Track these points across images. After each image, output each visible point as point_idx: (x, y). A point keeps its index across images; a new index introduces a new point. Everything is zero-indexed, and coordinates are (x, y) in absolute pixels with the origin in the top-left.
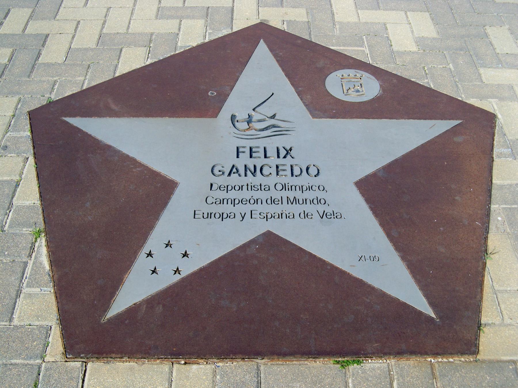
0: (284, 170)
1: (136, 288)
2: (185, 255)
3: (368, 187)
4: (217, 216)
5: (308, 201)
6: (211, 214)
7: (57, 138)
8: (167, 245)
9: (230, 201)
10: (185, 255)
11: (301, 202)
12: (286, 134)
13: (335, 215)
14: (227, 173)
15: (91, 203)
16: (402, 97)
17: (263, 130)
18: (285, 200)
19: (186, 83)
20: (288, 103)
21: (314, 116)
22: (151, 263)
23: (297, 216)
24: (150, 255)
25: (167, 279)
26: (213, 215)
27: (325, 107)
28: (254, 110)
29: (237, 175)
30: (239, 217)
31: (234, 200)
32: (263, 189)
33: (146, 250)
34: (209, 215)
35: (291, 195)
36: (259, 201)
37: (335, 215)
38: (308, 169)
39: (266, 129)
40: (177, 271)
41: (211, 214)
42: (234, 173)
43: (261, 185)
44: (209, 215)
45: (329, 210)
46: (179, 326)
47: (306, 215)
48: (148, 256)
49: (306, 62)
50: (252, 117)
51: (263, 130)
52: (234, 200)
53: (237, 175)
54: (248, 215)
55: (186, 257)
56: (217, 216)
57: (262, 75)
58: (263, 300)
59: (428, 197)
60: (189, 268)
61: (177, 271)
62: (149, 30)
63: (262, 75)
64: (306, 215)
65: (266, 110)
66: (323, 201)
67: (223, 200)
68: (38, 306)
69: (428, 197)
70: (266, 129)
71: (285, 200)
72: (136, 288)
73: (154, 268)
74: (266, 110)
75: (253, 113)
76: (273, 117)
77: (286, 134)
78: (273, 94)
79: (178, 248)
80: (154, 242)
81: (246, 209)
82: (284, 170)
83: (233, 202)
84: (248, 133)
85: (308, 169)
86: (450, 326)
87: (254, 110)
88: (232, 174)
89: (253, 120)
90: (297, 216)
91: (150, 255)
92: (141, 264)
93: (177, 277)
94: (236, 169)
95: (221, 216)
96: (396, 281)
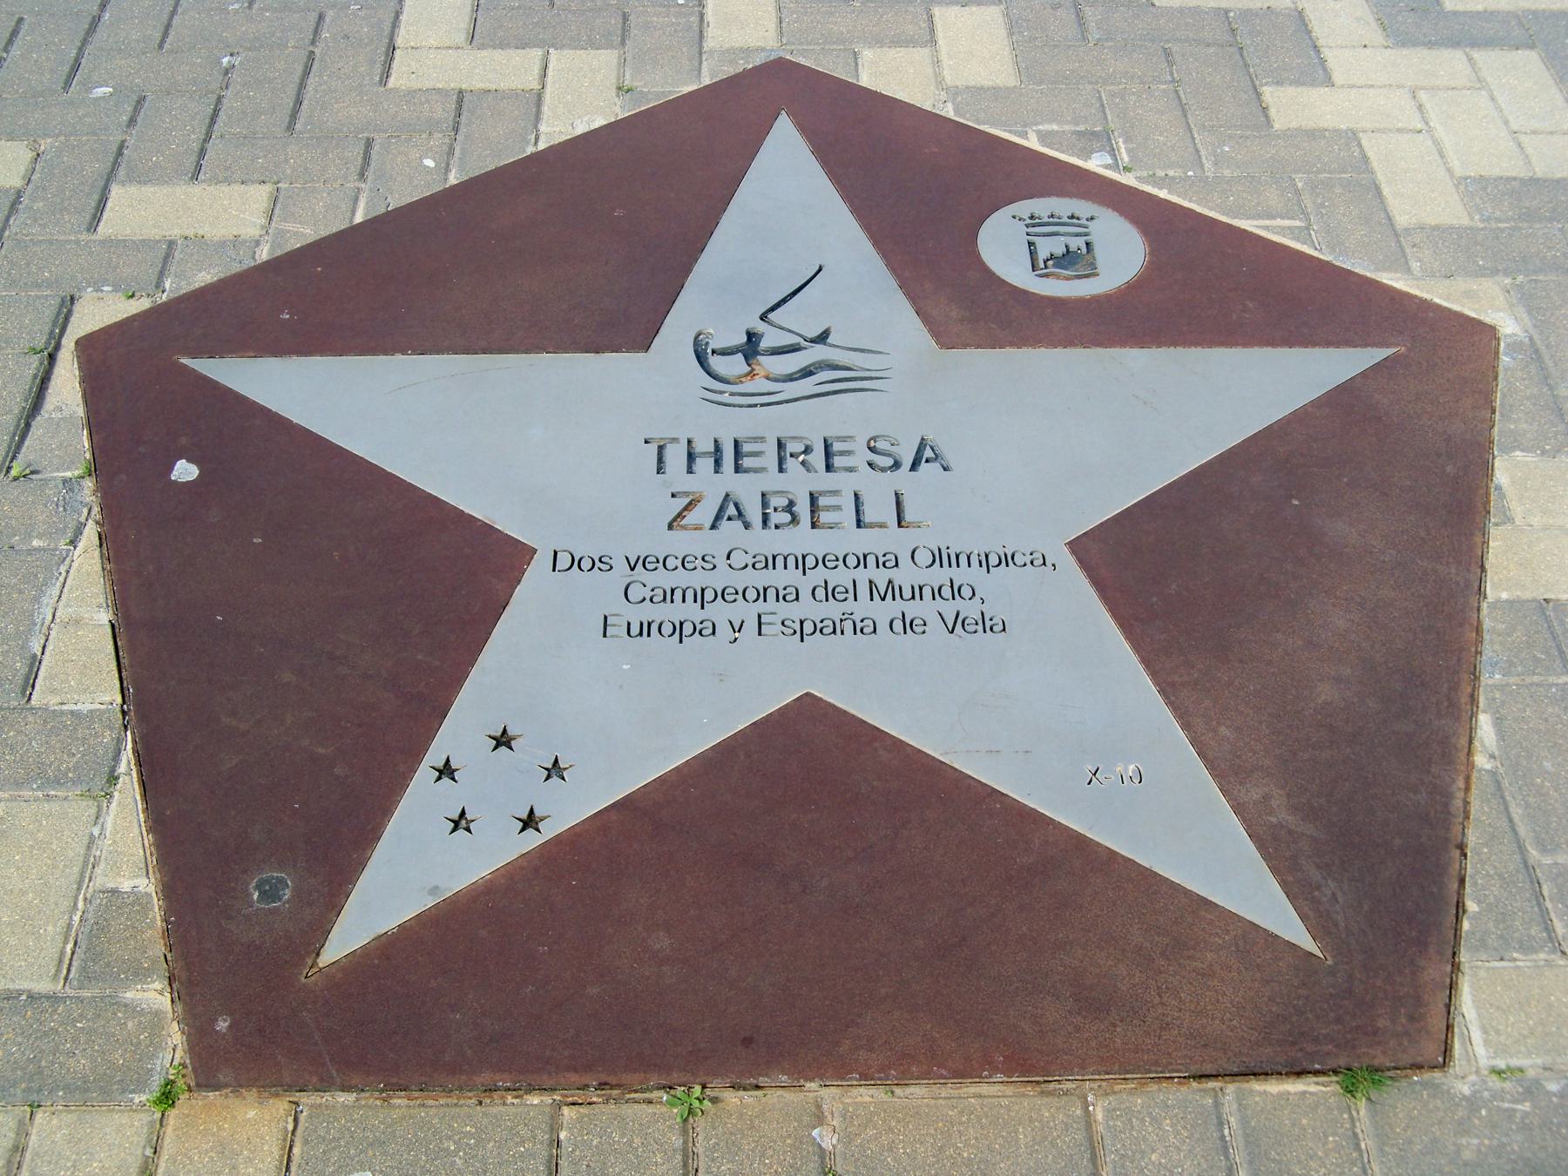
1: (415, 867)
2: (555, 770)
3: (535, 551)
4: (667, 629)
5: (927, 592)
6: (649, 624)
7: (160, 409)
9: (690, 595)
10: (555, 770)
11: (907, 594)
13: (985, 624)
14: (907, 462)
15: (282, 631)
16: (1209, 284)
17: (790, 378)
18: (863, 590)
19: (574, 244)
20: (863, 301)
21: (945, 337)
22: (451, 798)
23: (883, 627)
24: (446, 771)
25: (495, 850)
26: (654, 628)
28: (763, 317)
29: (738, 524)
30: (724, 631)
33: (434, 756)
34: (645, 629)
37: (985, 624)
39: (807, 373)
40: (530, 822)
41: (649, 624)
42: (730, 519)
44: (645, 629)
45: (971, 610)
46: (552, 978)
47: (909, 625)
48: (439, 778)
49: (924, 192)
51: (790, 378)
53: (936, 466)
54: (751, 625)
55: (461, 832)
56: (667, 629)
58: (813, 889)
60: (568, 810)
63: (788, 212)
64: (909, 625)
65: (799, 319)
66: (966, 592)
67: (641, 634)
69: (1292, 583)
70: (807, 373)
71: (863, 590)
72: (415, 867)
74: (799, 319)
75: (761, 327)
76: (822, 338)
78: (820, 270)
79: (561, 726)
80: (460, 733)
81: (746, 611)
83: (700, 597)
84: (748, 386)
86: (1365, 986)
87: (763, 317)
88: (724, 523)
89: (765, 344)
90: (883, 627)
91: (446, 771)
93: (532, 840)
95: (678, 628)
96: (1192, 835)
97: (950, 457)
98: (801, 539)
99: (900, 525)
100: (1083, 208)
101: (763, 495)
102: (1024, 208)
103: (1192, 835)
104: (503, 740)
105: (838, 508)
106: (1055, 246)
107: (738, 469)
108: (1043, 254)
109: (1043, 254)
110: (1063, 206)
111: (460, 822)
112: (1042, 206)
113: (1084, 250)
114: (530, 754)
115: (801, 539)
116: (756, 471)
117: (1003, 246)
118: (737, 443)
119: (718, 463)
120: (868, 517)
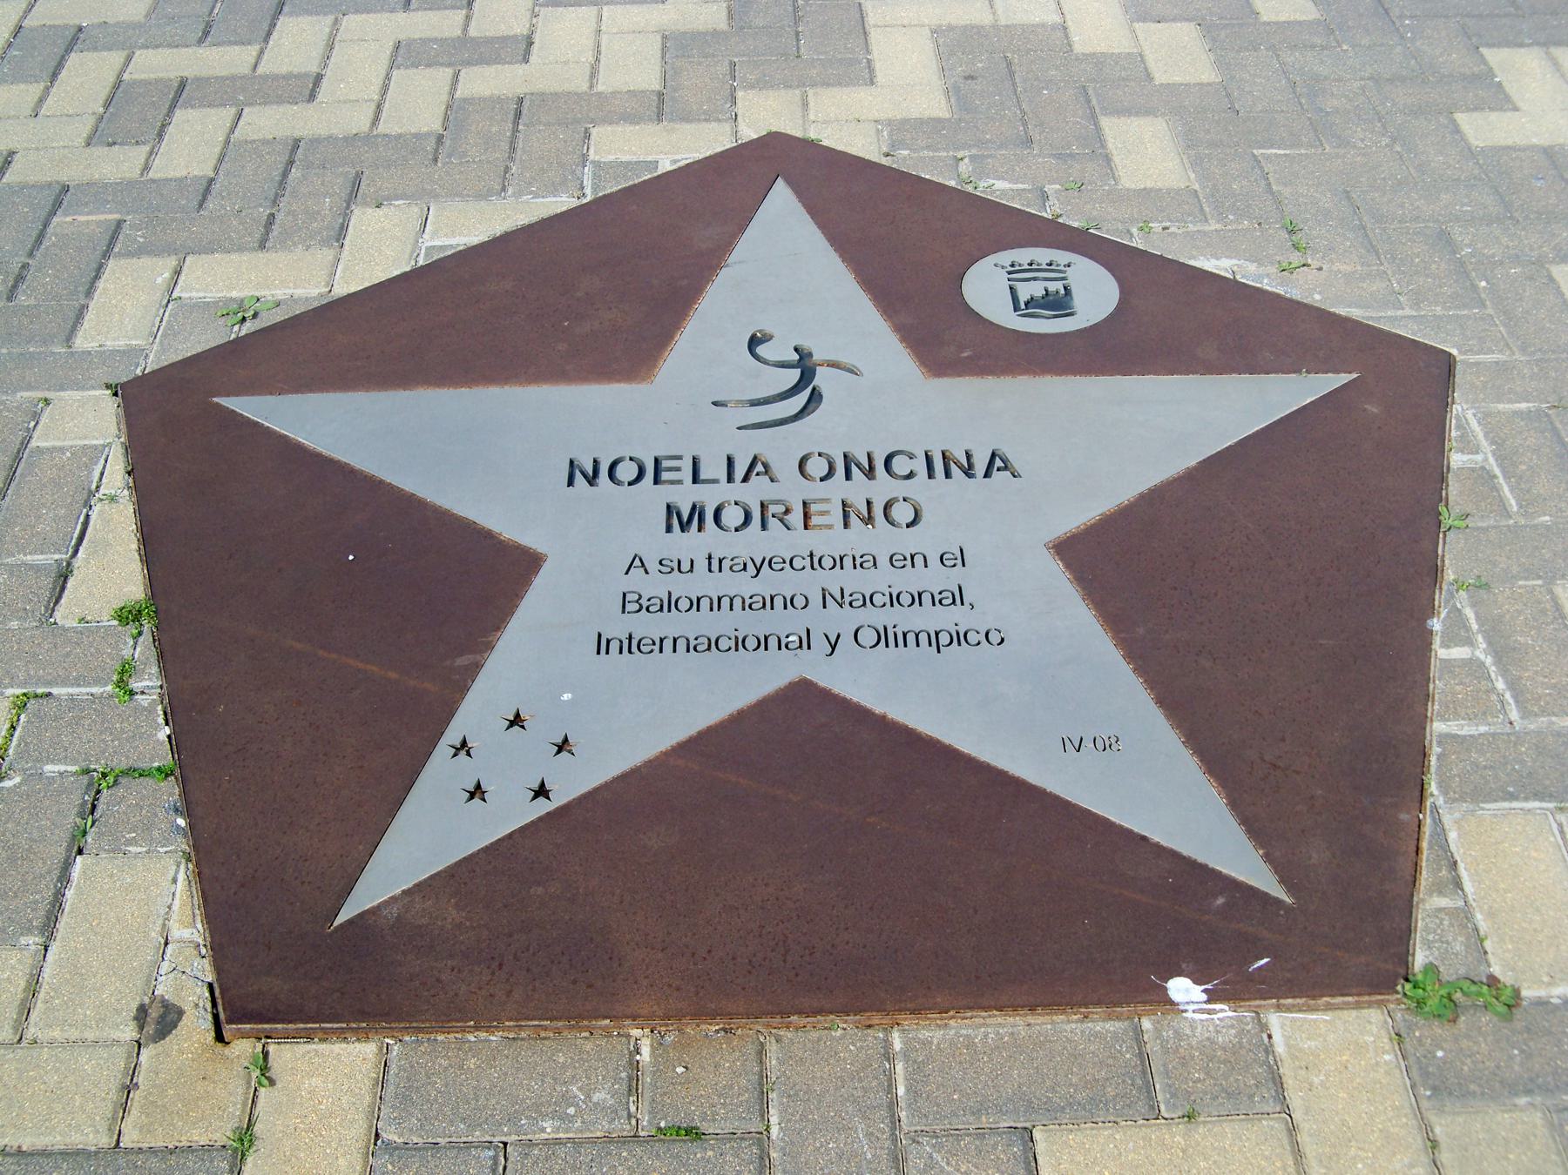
0: (822, 513)
1: (425, 838)
2: (563, 746)
5: (779, 602)
8: (512, 724)
9: (923, 638)
10: (563, 746)
12: (755, 403)
15: (295, 610)
16: (1174, 318)
19: (593, 287)
25: (512, 812)
27: (945, 338)
31: (937, 634)
32: (634, 648)
33: (452, 736)
35: (834, 581)
36: (919, 560)
38: (887, 507)
40: (542, 792)
43: (811, 555)
46: (566, 928)
47: (740, 643)
50: (810, 355)
52: (937, 634)
57: (784, 272)
58: (830, 867)
59: (1288, 595)
60: (573, 781)
61: (542, 792)
62: (174, 75)
63: (784, 272)
67: (719, 599)
68: (144, 907)
69: (1288, 595)
72: (425, 838)
73: (474, 783)
77: (755, 403)
79: (558, 714)
80: (476, 714)
82: (822, 513)
85: (887, 507)
86: (1338, 913)
92: (441, 773)
93: (543, 807)
94: (765, 465)
96: (1171, 802)
97: (1016, 464)
98: (797, 542)
99: (806, 528)
100: (1061, 257)
101: (804, 503)
102: (1006, 257)
103: (1171, 802)
104: (517, 721)
105: (678, 469)
106: (1037, 289)
107: (657, 481)
108: (1023, 297)
109: (1023, 297)
110: (1042, 255)
111: (477, 792)
112: (1023, 256)
113: (1062, 292)
114: (542, 733)
115: (797, 542)
116: (672, 482)
117: (987, 289)
118: (656, 460)
119: (931, 476)
120: (703, 476)
